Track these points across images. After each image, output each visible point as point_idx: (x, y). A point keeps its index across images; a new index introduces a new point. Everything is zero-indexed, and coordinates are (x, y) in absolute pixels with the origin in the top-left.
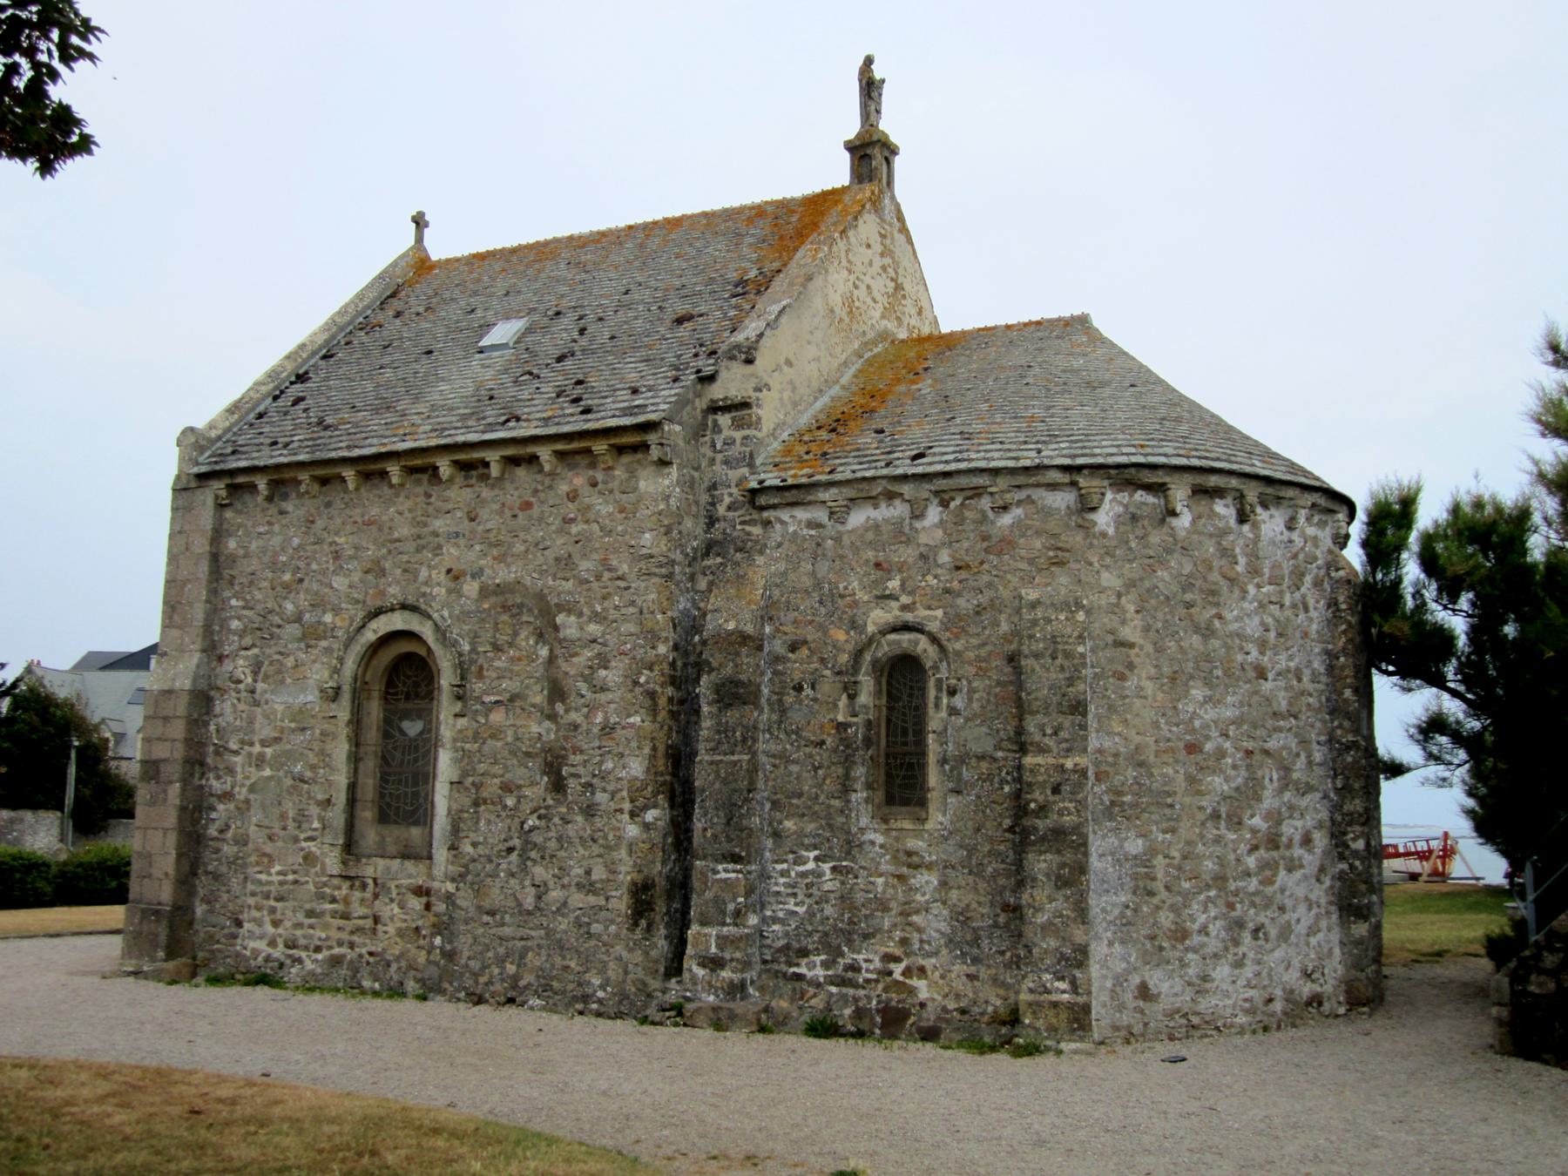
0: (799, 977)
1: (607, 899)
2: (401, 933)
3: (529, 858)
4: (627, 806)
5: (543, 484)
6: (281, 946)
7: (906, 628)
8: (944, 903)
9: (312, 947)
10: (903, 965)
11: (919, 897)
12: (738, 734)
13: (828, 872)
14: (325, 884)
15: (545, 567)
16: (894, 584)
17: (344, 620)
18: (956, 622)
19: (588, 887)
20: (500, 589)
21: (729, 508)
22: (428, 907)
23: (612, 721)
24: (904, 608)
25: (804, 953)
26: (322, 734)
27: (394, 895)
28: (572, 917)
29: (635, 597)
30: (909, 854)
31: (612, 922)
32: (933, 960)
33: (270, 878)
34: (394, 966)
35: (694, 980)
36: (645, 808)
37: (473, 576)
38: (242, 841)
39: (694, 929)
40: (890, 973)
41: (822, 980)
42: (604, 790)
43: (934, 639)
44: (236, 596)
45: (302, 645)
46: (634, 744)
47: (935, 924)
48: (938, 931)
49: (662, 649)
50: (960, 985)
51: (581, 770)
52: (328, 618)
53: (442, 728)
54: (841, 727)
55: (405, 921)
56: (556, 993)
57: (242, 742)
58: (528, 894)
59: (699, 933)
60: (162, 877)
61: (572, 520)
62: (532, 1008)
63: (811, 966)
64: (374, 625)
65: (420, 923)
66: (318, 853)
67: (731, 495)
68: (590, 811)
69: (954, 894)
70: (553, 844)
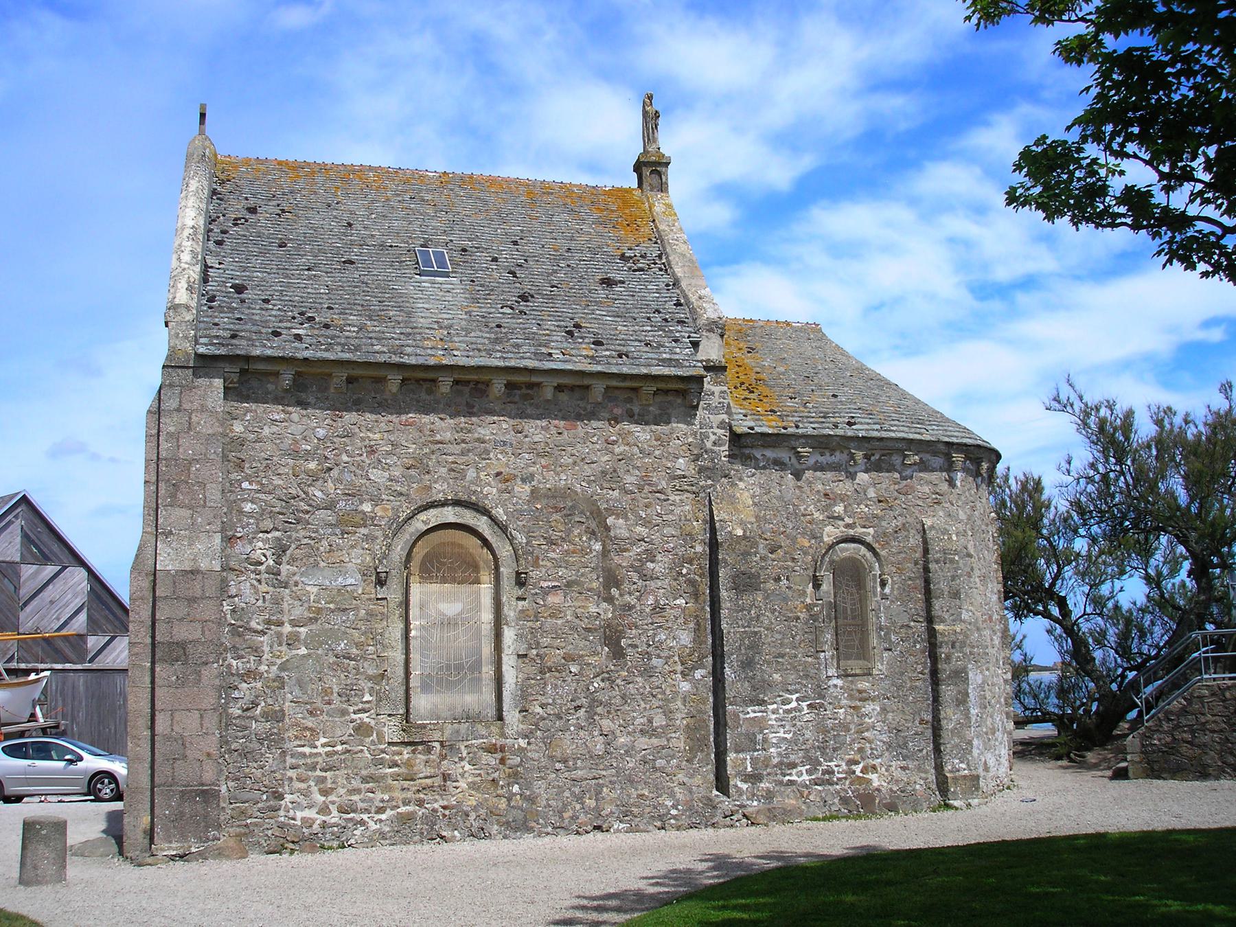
0: (792, 783)
1: (668, 740)
2: (472, 786)
3: (596, 714)
4: (679, 668)
5: (585, 409)
6: (335, 813)
7: (853, 540)
8: (884, 722)
9: (373, 810)
10: (861, 766)
11: (867, 720)
12: (753, 612)
13: (806, 708)
14: (383, 751)
15: (592, 478)
16: (839, 509)
17: (386, 510)
18: (882, 536)
19: (649, 731)
20: (554, 494)
21: (715, 443)
22: (502, 761)
23: (662, 603)
24: (848, 526)
25: (793, 765)
26: (367, 614)
27: (464, 755)
28: (638, 757)
29: (673, 507)
30: (860, 692)
31: (673, 757)
32: (879, 760)
33: (315, 751)
34: (473, 815)
35: (739, 790)
36: (694, 668)
37: (523, 480)
38: (277, 716)
39: (731, 757)
40: (854, 772)
41: (808, 783)
42: (659, 657)
43: (870, 547)
44: (248, 478)
45: (338, 531)
46: (681, 620)
47: (879, 737)
48: (881, 741)
49: (699, 549)
50: (898, 774)
51: (637, 642)
52: (367, 507)
53: (506, 609)
54: (809, 608)
55: (480, 775)
56: (636, 817)
57: (268, 622)
58: (598, 742)
59: (735, 758)
60: (203, 758)
61: (614, 443)
62: (618, 831)
63: (800, 774)
64: (423, 516)
65: (496, 775)
66: (373, 723)
67: (715, 434)
68: (648, 672)
69: (890, 716)
70: (618, 701)
